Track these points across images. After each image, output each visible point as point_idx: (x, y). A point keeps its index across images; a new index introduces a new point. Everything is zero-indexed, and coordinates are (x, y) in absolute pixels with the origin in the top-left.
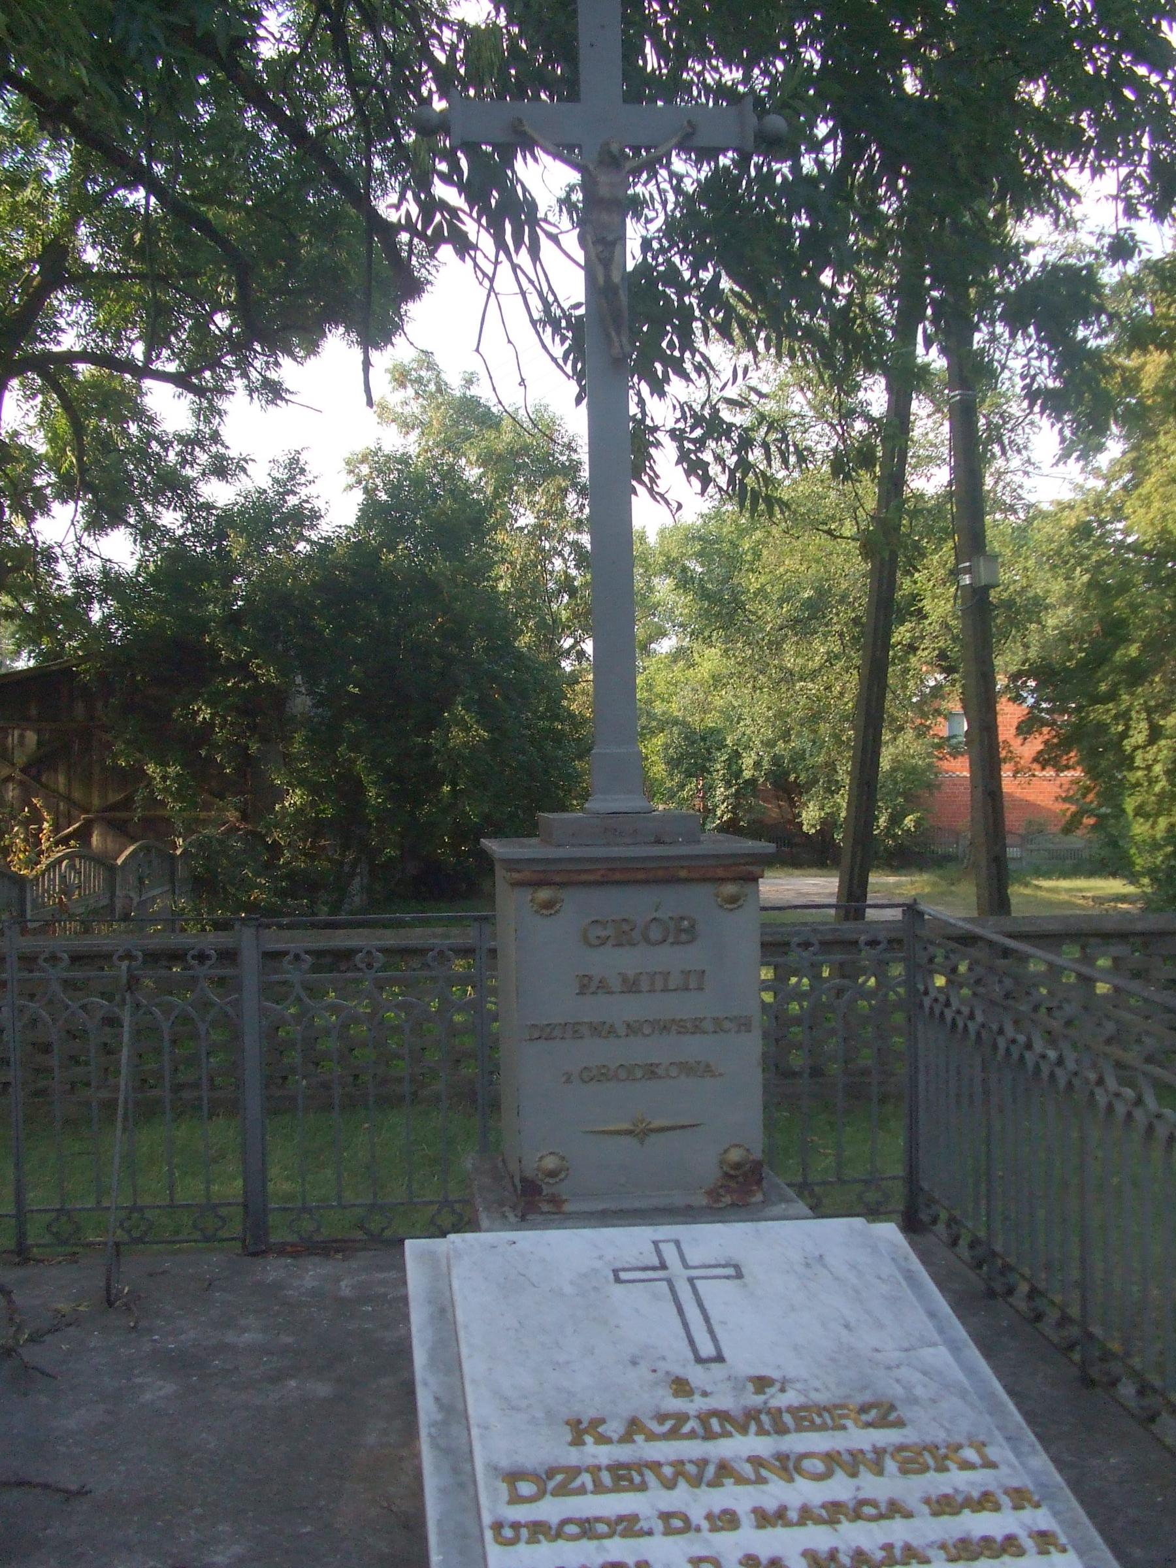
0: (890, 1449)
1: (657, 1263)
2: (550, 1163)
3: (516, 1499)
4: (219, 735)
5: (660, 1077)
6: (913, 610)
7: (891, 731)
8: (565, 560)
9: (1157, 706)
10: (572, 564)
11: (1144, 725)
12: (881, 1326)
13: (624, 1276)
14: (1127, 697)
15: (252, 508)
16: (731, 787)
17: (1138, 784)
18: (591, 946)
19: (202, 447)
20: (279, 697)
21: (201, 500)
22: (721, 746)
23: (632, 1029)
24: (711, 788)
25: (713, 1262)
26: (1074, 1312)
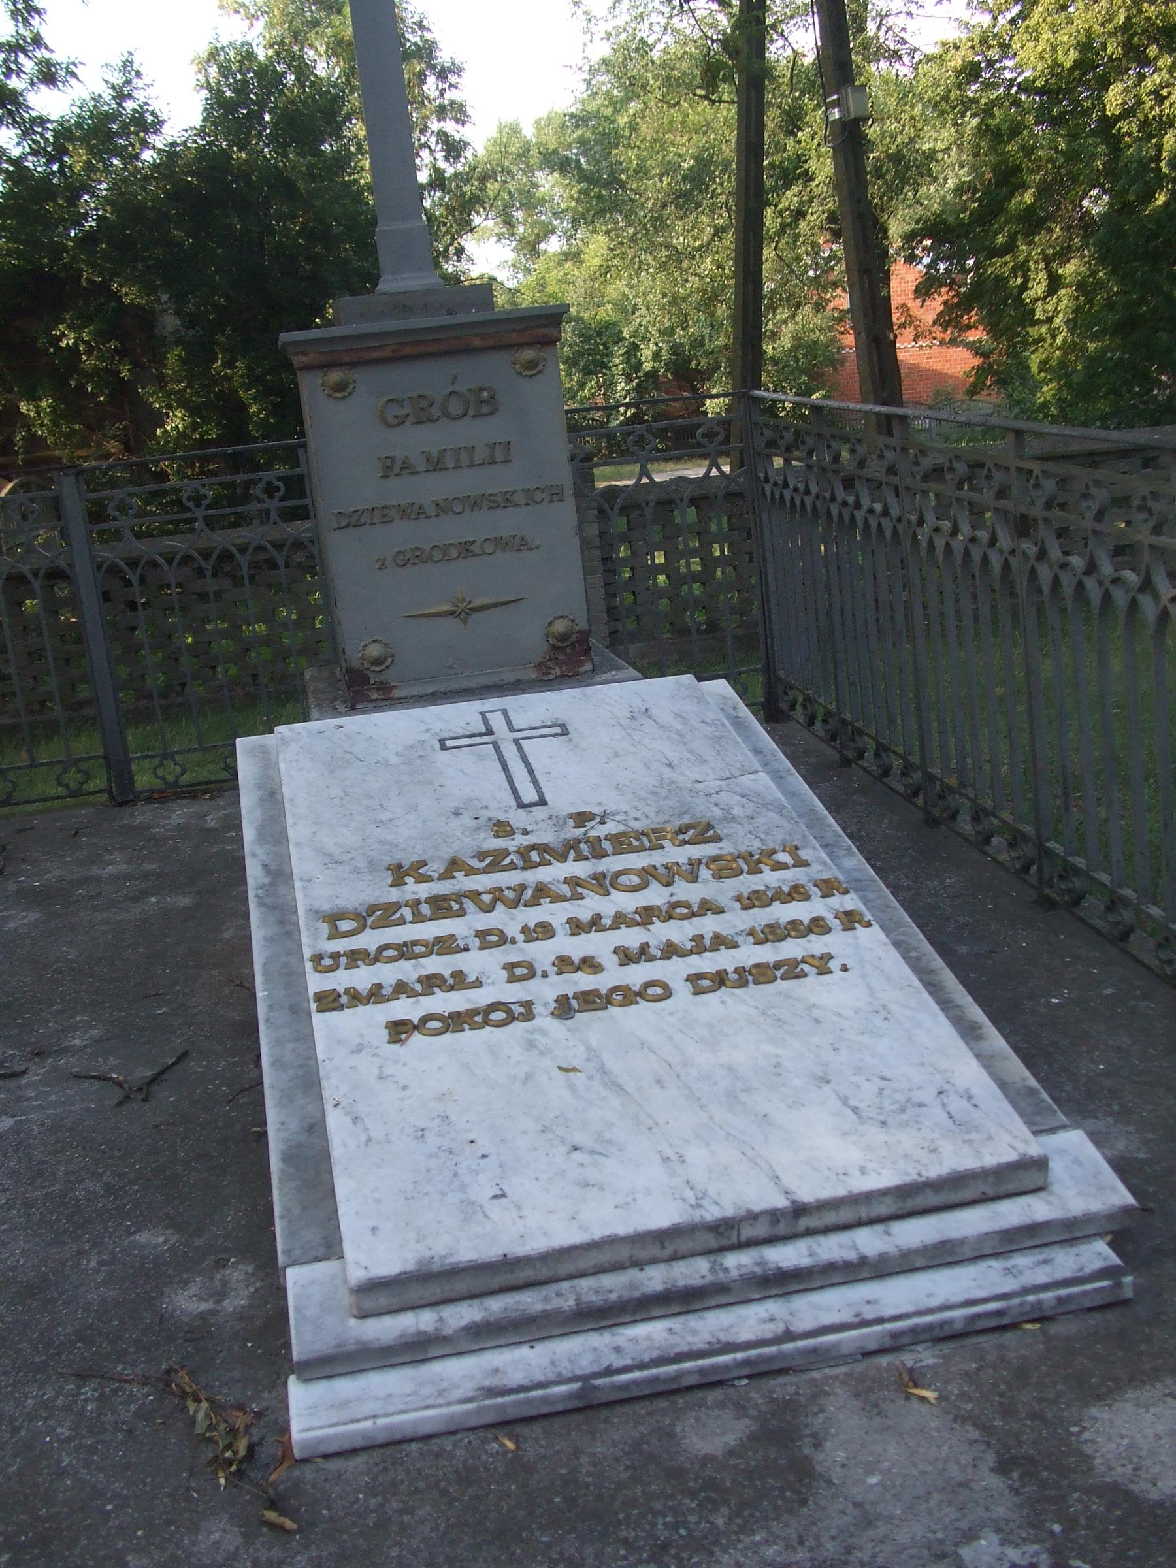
0: (704, 861)
1: (484, 730)
2: (375, 651)
3: (335, 935)
4: (89, 362)
5: (475, 555)
6: (795, 173)
7: (790, 308)
8: (432, 152)
9: (1055, 255)
10: (440, 155)
11: (1043, 275)
12: (702, 761)
13: (449, 743)
14: (1024, 247)
15: (90, 118)
16: (632, 381)
17: (1041, 339)
18: (390, 426)
19: (25, 52)
21: (34, 114)
22: (619, 340)
23: (442, 508)
24: (610, 385)
25: (540, 724)
26: (915, 759)
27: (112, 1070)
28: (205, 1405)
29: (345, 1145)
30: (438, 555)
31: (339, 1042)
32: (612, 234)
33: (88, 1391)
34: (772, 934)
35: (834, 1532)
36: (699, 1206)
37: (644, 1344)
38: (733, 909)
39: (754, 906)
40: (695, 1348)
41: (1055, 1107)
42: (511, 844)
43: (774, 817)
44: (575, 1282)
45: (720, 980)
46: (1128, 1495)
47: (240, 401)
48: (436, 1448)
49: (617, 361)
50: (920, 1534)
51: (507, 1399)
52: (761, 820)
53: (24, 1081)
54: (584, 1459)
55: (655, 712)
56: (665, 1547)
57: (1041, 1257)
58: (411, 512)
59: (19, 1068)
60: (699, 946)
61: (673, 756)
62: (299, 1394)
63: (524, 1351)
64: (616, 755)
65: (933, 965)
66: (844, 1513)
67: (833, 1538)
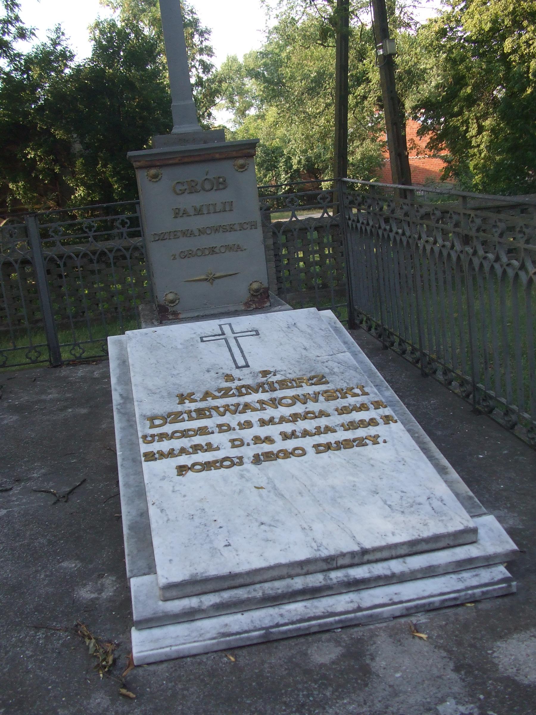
0: (321, 393)
1: (220, 333)
2: (171, 297)
3: (153, 426)
4: (40, 165)
5: (217, 253)
6: (362, 79)
7: (360, 140)
8: (197, 69)
9: (481, 116)
10: (201, 71)
11: (475, 126)
12: (320, 347)
13: (205, 339)
14: (467, 113)
15: (41, 54)
16: (288, 174)
17: (475, 155)
18: (178, 194)
19: (11, 24)
20: (66, 145)
21: (15, 52)
22: (282, 155)
23: (202, 232)
24: (278, 175)
25: (246, 330)
26: (417, 346)
27: (51, 488)
28: (93, 641)
29: (157, 522)
30: (199, 253)
31: (154, 475)
32: (279, 107)
33: (40, 634)
34: (352, 426)
35: (380, 699)
36: (319, 550)
37: (293, 613)
38: (334, 415)
39: (344, 413)
40: (317, 615)
41: (481, 505)
42: (233, 385)
43: (353, 373)
44: (262, 584)
45: (328, 447)
46: (514, 682)
47: (109, 183)
48: (199, 660)
49: (281, 164)
50: (419, 700)
51: (231, 638)
52: (347, 374)
53: (11, 493)
54: (266, 665)
55: (298, 325)
56: (303, 705)
57: (474, 573)
58: (188, 234)
59: (8, 487)
60: (319, 431)
61: (307, 345)
62: (136, 636)
63: (239, 616)
64: (281, 344)
65: (425, 440)
66: (385, 690)
67: (380, 701)
